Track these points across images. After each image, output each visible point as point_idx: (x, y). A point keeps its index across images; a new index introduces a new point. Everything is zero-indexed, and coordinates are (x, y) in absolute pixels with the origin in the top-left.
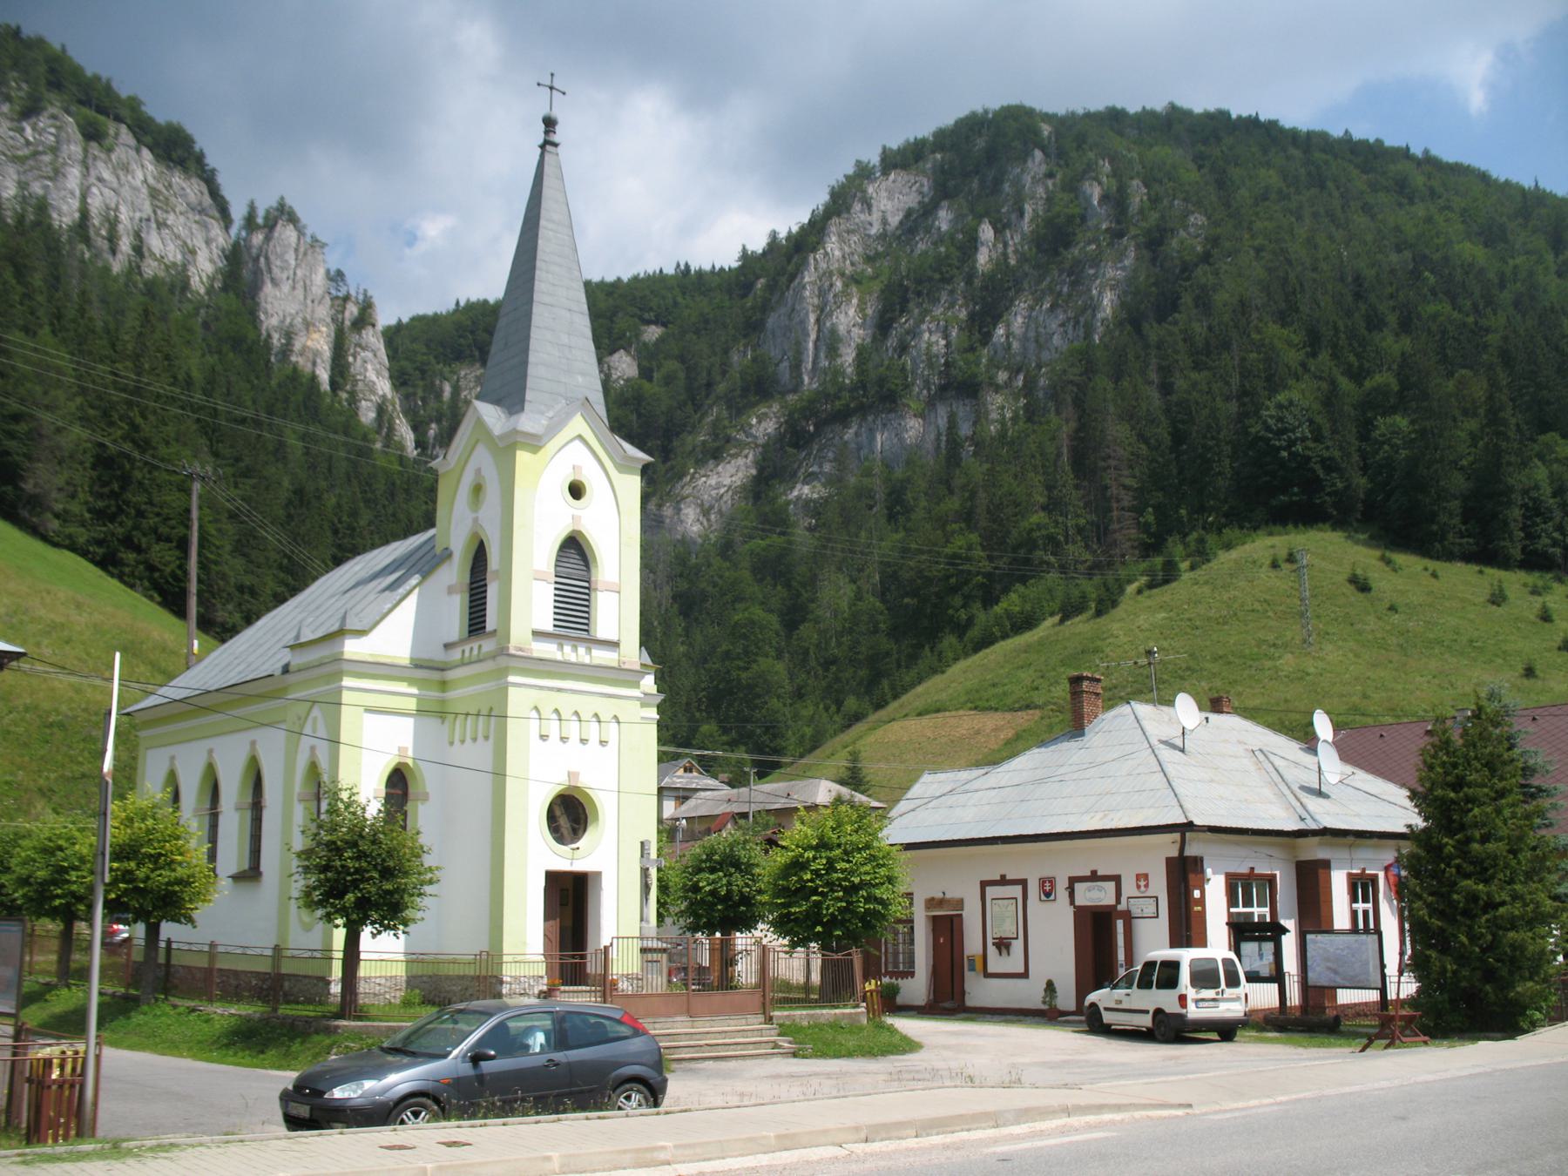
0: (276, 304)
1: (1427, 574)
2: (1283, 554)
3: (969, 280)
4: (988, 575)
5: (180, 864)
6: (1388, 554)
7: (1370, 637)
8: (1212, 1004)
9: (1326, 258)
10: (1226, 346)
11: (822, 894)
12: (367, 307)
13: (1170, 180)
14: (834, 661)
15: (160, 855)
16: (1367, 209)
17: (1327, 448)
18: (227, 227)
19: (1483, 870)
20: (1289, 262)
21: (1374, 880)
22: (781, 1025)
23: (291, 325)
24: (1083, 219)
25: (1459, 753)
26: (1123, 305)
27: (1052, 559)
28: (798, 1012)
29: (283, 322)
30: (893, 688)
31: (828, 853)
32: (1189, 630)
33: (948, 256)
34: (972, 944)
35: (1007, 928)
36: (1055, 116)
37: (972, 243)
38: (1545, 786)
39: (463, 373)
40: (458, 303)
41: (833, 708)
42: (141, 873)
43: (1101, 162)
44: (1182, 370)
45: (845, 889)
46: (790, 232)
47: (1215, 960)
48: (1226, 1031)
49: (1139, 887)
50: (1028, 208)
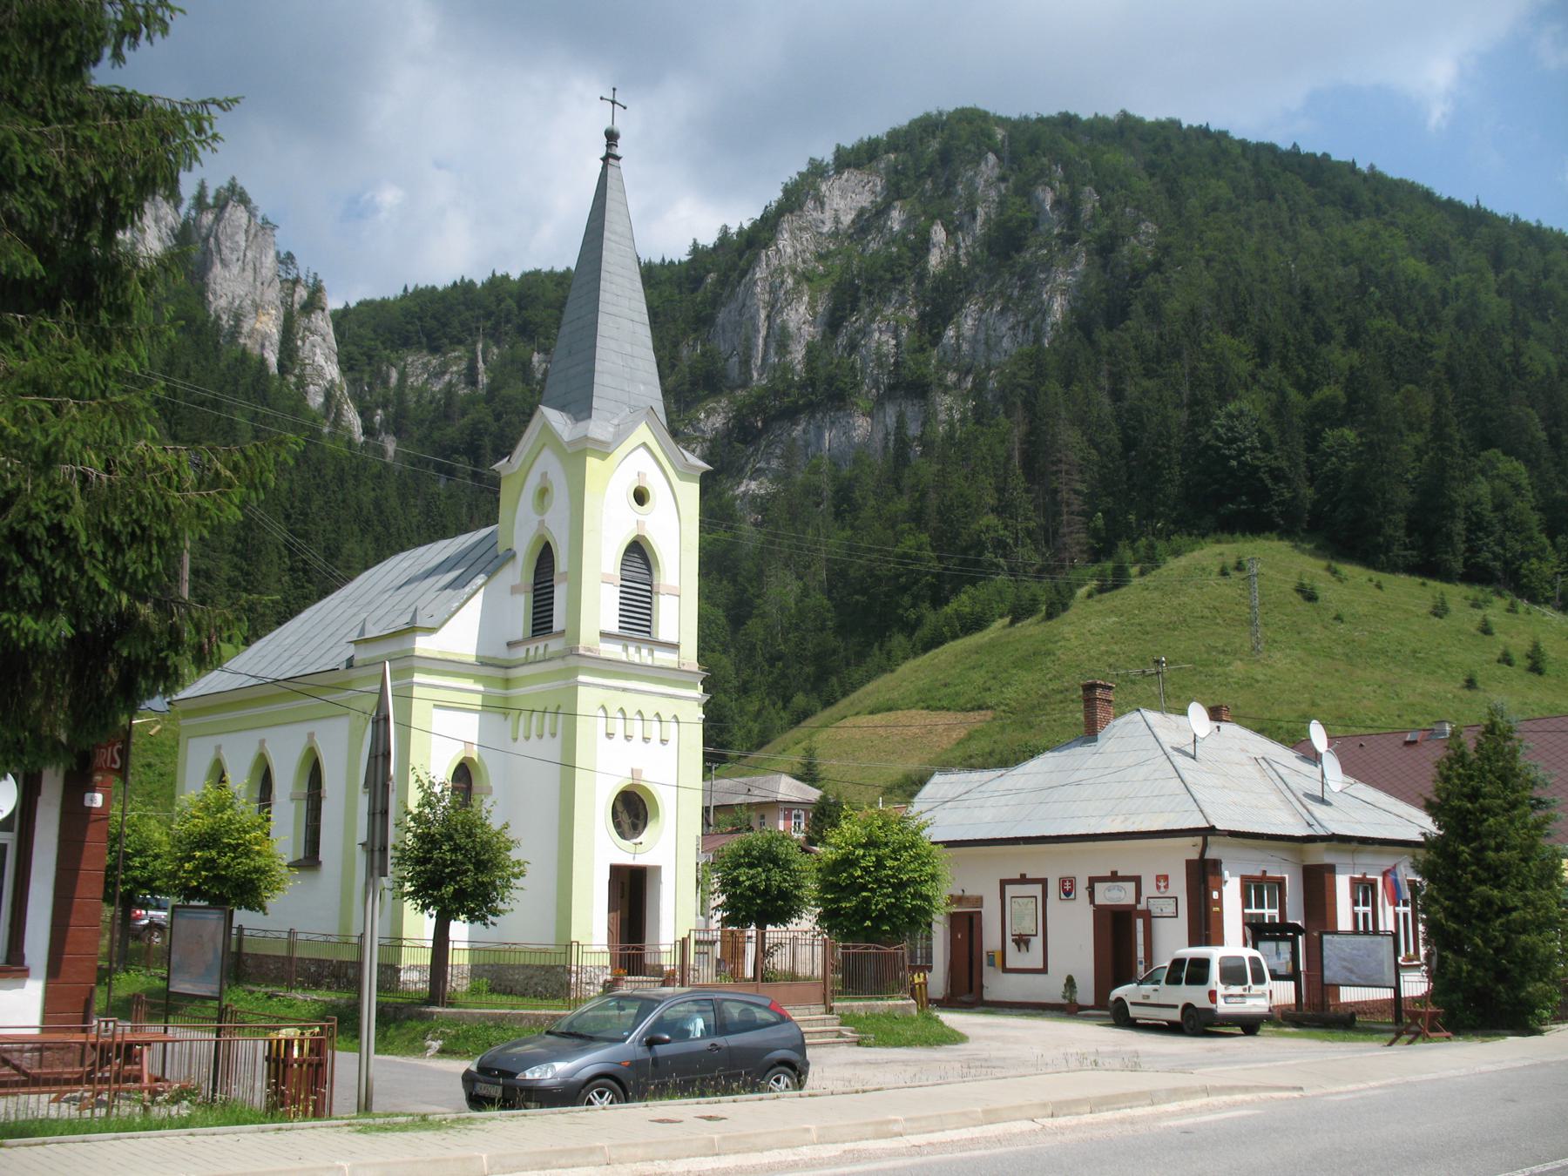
0: (225, 285)
1: (1372, 585)
2: (1232, 561)
3: (920, 280)
4: (937, 576)
5: (259, 853)
6: (1334, 564)
7: (1317, 646)
8: (1239, 999)
9: (1276, 270)
10: (1177, 354)
11: (871, 890)
12: (316, 291)
13: (1121, 187)
14: (780, 657)
15: (239, 845)
16: (1314, 222)
17: (1276, 458)
18: (177, 207)
19: (1497, 876)
20: (1239, 273)
21: (1373, 884)
22: (842, 1015)
23: (240, 306)
24: (1036, 223)
25: (1475, 766)
26: (1073, 310)
27: (1002, 561)
28: (856, 1004)
29: (232, 303)
30: (841, 684)
31: (876, 851)
32: (1139, 635)
33: (899, 257)
34: (991, 939)
35: (1027, 926)
36: (1008, 120)
37: (924, 245)
38: (1545, 798)
39: (410, 360)
40: (406, 289)
41: (780, 704)
42: (224, 861)
43: (1054, 167)
44: (1132, 377)
45: (892, 886)
46: (741, 227)
47: (1242, 958)
48: (1249, 1025)
49: (1158, 887)
50: (980, 211)
